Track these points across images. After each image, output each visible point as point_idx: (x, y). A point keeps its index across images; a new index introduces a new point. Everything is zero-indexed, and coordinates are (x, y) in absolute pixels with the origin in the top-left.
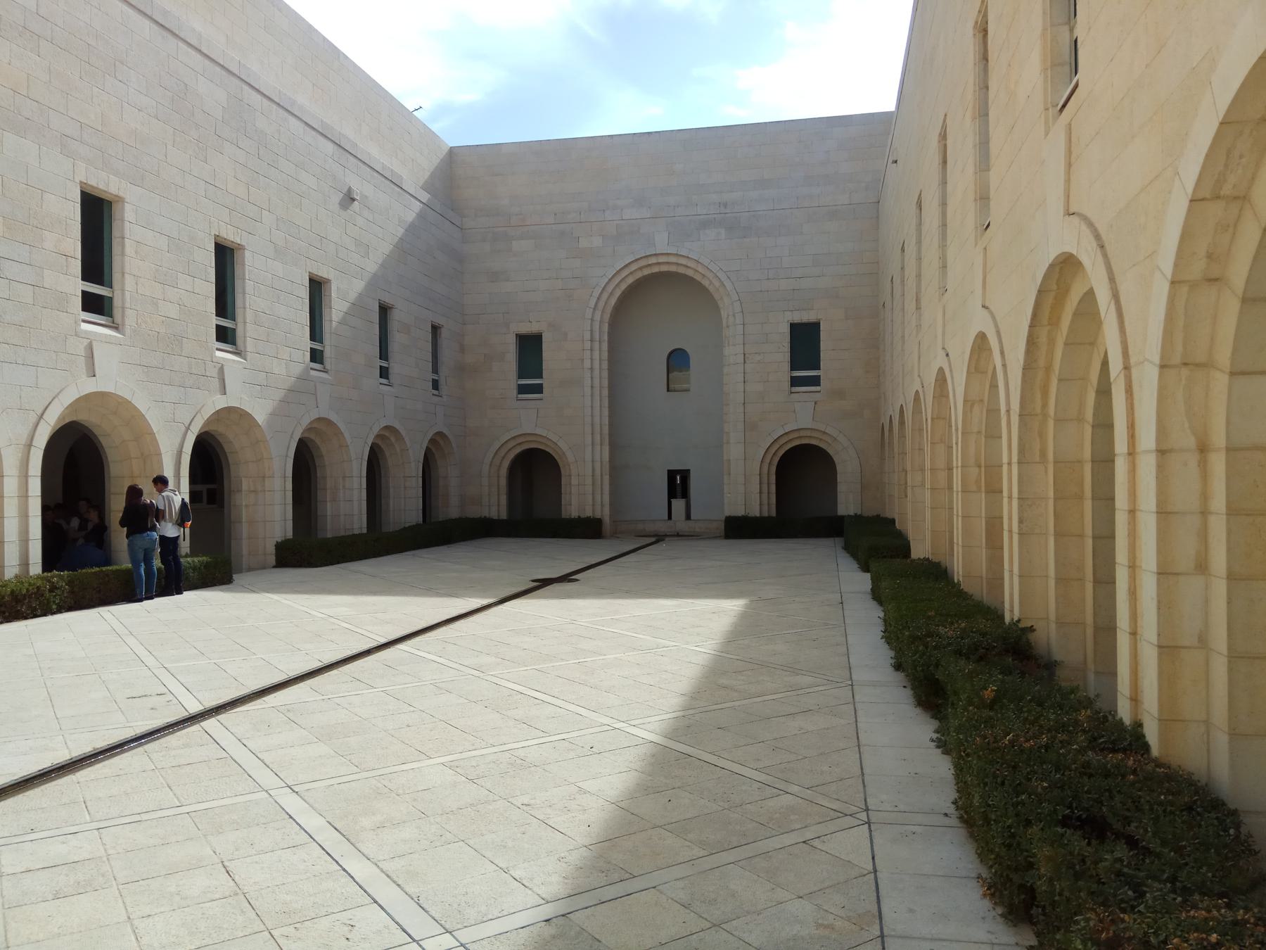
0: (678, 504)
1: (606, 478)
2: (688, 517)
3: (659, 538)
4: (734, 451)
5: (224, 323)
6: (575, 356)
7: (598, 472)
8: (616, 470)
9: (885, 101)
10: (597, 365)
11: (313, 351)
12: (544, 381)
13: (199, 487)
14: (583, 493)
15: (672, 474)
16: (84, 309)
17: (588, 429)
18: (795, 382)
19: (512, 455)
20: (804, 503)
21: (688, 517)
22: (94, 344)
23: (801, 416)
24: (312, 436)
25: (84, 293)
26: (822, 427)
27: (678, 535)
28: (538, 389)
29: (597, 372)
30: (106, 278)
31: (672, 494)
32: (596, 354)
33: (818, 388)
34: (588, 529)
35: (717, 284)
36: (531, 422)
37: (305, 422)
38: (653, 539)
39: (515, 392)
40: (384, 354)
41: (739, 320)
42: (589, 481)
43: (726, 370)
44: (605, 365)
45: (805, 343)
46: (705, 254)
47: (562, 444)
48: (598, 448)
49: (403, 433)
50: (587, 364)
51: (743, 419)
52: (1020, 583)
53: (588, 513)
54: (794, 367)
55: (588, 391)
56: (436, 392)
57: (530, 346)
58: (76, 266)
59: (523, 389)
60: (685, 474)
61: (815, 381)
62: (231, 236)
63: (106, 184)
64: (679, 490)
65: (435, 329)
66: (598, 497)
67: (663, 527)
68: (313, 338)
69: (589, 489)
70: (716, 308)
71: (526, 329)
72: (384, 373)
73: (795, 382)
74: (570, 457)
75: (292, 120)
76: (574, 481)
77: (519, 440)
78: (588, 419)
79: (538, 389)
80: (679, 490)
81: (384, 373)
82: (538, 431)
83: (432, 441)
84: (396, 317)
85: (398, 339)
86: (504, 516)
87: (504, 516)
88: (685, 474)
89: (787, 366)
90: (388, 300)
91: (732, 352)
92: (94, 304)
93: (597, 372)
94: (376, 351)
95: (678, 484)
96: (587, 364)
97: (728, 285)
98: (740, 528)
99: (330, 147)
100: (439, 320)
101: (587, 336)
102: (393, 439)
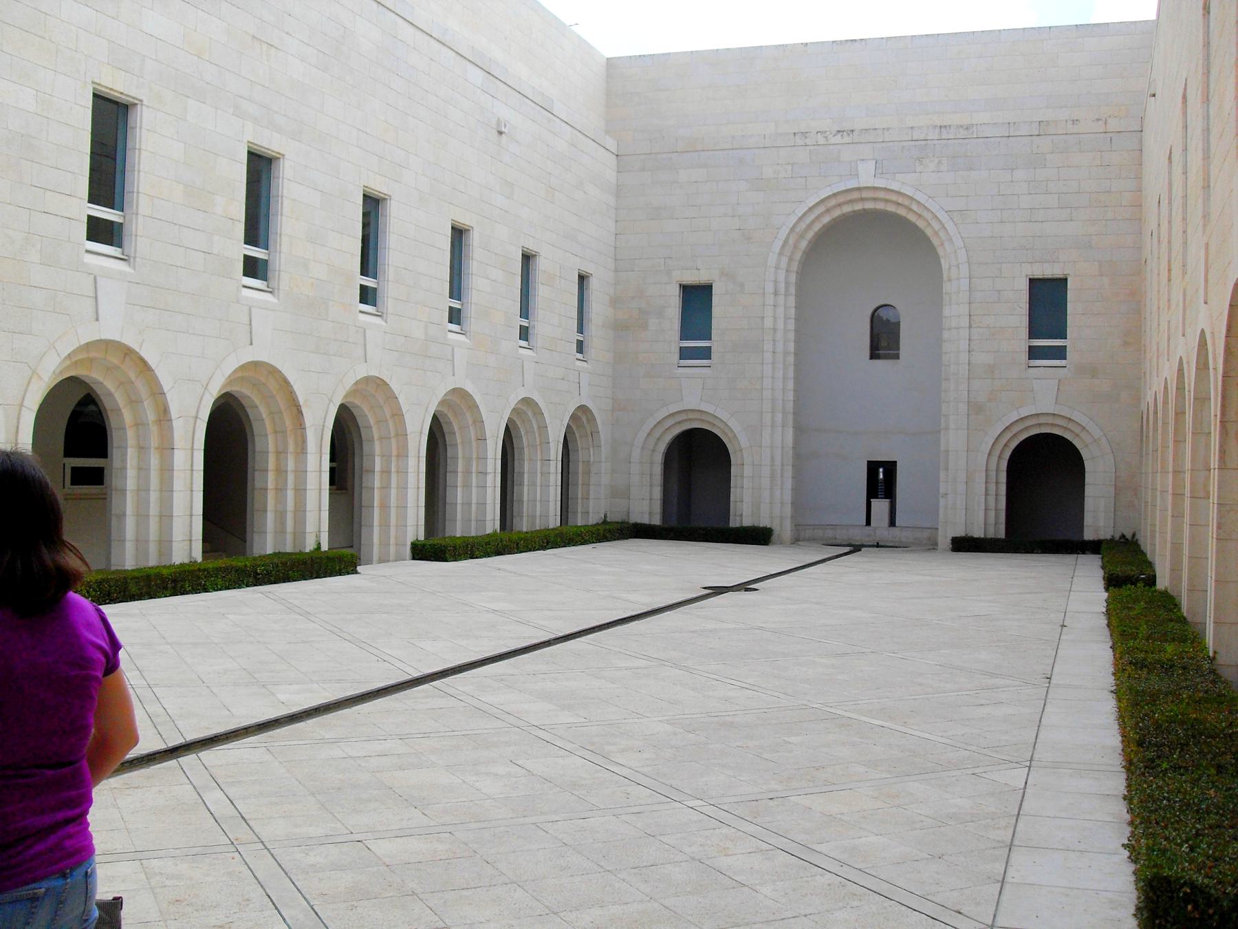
0: (880, 506)
2: (892, 523)
3: (856, 548)
4: (954, 439)
5: (369, 282)
6: (757, 308)
7: (778, 462)
8: (801, 459)
9: (1151, 15)
10: (781, 325)
11: (363, 289)
12: (715, 343)
13: (334, 465)
14: (755, 491)
15: (873, 467)
16: (89, 238)
18: (1034, 353)
19: (669, 437)
20: (1041, 496)
21: (892, 523)
22: (98, 279)
23: (1042, 398)
24: (358, 402)
25: (90, 218)
26: (1065, 412)
27: (878, 546)
28: (706, 353)
29: (780, 335)
30: (262, 239)
31: (873, 490)
32: (781, 310)
33: (1062, 363)
34: (758, 536)
35: (936, 226)
36: (698, 396)
37: (349, 382)
38: (847, 549)
39: (677, 356)
40: (525, 312)
41: (964, 270)
42: (766, 471)
43: (946, 335)
44: (791, 325)
45: (1047, 302)
46: (923, 189)
47: (732, 423)
49: (478, 399)
50: (768, 323)
51: (971, 398)
52: (1219, 551)
54: (1032, 334)
55: (768, 357)
56: (579, 356)
57: (696, 299)
58: (240, 230)
59: (685, 354)
60: (890, 467)
61: (1060, 353)
62: (379, 187)
63: (269, 143)
64: (881, 487)
65: (582, 278)
66: (778, 493)
67: (859, 535)
68: (364, 271)
70: (937, 258)
71: (691, 278)
72: (524, 333)
73: (1034, 353)
74: (743, 441)
75: (446, 50)
76: (748, 471)
80: (881, 487)
81: (524, 333)
83: (574, 417)
84: (542, 266)
85: (542, 292)
88: (890, 467)
89: (1025, 332)
90: (532, 246)
91: (955, 312)
92: (253, 268)
93: (780, 335)
94: (574, 324)
95: (881, 480)
97: (950, 226)
98: (964, 545)
99: (476, 76)
100: (587, 268)
101: (770, 288)
102: (530, 414)
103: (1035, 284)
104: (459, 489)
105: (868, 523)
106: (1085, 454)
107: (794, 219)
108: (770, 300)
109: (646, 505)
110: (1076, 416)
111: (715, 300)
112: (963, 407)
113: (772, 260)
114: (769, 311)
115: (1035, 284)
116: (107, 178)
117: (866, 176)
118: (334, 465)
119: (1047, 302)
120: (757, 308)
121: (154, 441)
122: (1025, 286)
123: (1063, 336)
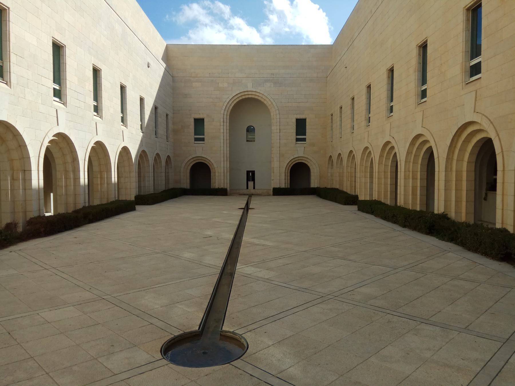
0: (251, 184)
1: (228, 173)
2: (254, 188)
4: (276, 164)
6: (217, 127)
8: (232, 170)
12: (206, 137)
13: (494, 177)
15: (248, 172)
17: (222, 155)
18: (298, 140)
21: (254, 188)
28: (203, 140)
34: (222, 192)
39: (194, 140)
42: (222, 174)
45: (301, 126)
46: (265, 92)
48: (225, 162)
53: (222, 186)
54: (297, 134)
55: (222, 141)
57: (199, 123)
59: (196, 140)
60: (253, 172)
66: (226, 181)
69: (222, 178)
71: (198, 116)
76: (217, 174)
77: (195, 159)
78: (222, 152)
79: (203, 140)
80: (251, 178)
82: (203, 156)
86: (188, 187)
87: (188, 187)
89: (295, 134)
95: (251, 176)
96: (222, 131)
98: (278, 192)
103: (298, 120)
104: (389, 183)
105: (247, 188)
106: (311, 168)
107: (228, 100)
108: (222, 124)
109: (186, 184)
110: (309, 157)
111: (205, 123)
112: (278, 155)
113: (222, 112)
114: (222, 127)
115: (298, 120)
116: (58, 75)
117: (250, 87)
118: (494, 177)
119: (301, 126)
120: (217, 127)
121: (70, 169)
122: (294, 121)
123: (204, 135)
